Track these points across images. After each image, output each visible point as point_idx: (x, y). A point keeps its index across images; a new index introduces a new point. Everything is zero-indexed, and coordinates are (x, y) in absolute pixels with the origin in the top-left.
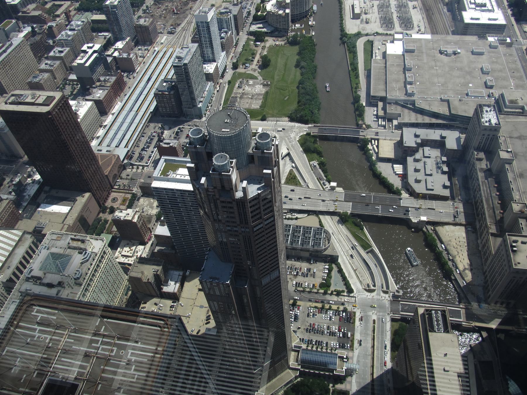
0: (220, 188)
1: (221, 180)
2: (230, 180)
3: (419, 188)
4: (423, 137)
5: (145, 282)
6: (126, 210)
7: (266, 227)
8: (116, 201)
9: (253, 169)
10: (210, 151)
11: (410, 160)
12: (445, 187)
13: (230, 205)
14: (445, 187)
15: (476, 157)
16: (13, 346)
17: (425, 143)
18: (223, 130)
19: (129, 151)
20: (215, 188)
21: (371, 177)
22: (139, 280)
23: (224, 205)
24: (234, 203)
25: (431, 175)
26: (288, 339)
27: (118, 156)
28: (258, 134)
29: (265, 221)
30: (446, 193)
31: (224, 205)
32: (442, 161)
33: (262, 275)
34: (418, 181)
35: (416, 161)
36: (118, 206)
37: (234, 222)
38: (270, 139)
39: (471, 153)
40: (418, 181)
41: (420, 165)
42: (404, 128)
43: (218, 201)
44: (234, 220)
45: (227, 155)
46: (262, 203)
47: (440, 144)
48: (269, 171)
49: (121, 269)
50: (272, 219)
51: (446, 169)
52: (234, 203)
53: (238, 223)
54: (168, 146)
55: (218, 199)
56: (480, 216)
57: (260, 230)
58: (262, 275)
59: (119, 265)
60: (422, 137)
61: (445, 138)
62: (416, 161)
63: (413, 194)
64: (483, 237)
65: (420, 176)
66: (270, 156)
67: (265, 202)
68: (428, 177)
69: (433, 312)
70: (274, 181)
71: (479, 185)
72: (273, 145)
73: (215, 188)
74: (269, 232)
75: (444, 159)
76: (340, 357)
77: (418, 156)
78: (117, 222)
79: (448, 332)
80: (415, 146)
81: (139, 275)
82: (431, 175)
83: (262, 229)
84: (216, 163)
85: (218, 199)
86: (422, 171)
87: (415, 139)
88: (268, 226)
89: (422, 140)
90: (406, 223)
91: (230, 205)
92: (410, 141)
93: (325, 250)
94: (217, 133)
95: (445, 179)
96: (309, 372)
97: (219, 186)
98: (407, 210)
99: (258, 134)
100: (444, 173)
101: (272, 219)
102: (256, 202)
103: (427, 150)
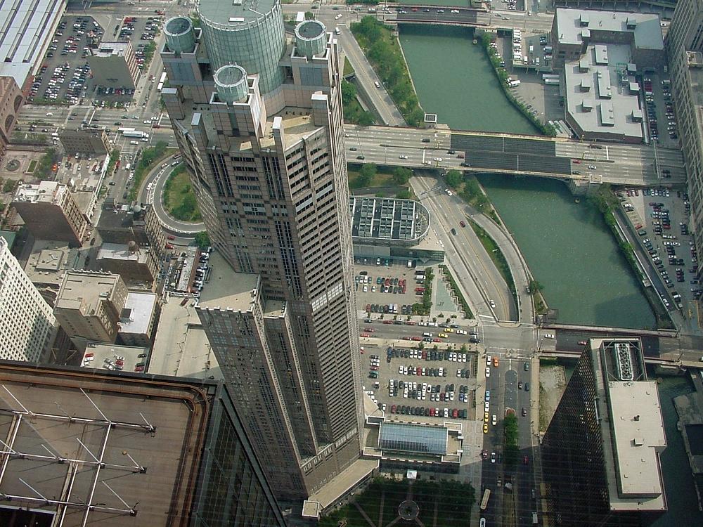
0: (230, 133)
1: (232, 117)
2: (249, 117)
3: (588, 123)
4: (594, 26)
5: (87, 318)
6: (38, 183)
7: (319, 204)
8: (16, 168)
9: (292, 93)
10: (206, 62)
11: (569, 68)
12: (635, 120)
13: (250, 165)
14: (635, 120)
15: (689, 63)
16: (639, 252)
17: (598, 37)
18: (231, 19)
19: (32, 69)
20: (220, 132)
21: (506, 104)
22: (76, 313)
23: (238, 164)
24: (256, 159)
25: (608, 98)
26: (359, 405)
27: (13, 80)
28: (298, 26)
29: (317, 192)
30: (635, 131)
31: (238, 164)
32: (630, 73)
33: (313, 295)
34: (586, 110)
35: (583, 71)
36: (20, 177)
37: (257, 197)
38: (322, 35)
39: (679, 57)
40: (586, 110)
41: (587, 81)
42: (558, 9)
43: (226, 159)
44: (257, 193)
45: (242, 69)
46: (311, 158)
47: (624, 39)
48: (325, 97)
49: (39, 295)
50: (330, 188)
51: (635, 86)
52: (256, 159)
53: (267, 198)
54: (109, 55)
55: (227, 154)
56: (695, 172)
57: (308, 211)
58: (313, 295)
59: (35, 289)
60: (592, 26)
61: (633, 27)
62: (583, 71)
63: (577, 135)
64: (698, 210)
65: (590, 100)
66: (323, 66)
67: (316, 156)
68: (603, 102)
69: (617, 345)
70: (331, 116)
71: (693, 115)
72: (329, 46)
73: (220, 132)
74: (324, 214)
75: (632, 67)
76: (450, 433)
77: (585, 62)
78: (23, 208)
79: (641, 379)
80: (580, 43)
81: (74, 305)
82: (608, 98)
83: (312, 209)
84: (222, 85)
85: (227, 154)
86: (592, 91)
87: (579, 30)
88: (323, 201)
89: (592, 31)
90: (563, 188)
91: (250, 165)
92: (569, 35)
93: (418, 242)
94: (219, 26)
95: (632, 106)
96: (398, 461)
97: (228, 128)
98: (564, 164)
99: (298, 26)
100: (633, 93)
101: (330, 188)
102: (299, 156)
103: (602, 52)
